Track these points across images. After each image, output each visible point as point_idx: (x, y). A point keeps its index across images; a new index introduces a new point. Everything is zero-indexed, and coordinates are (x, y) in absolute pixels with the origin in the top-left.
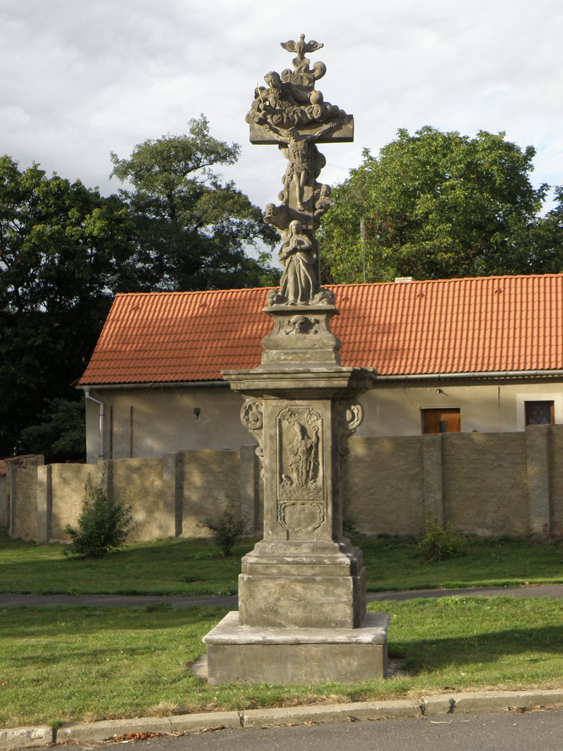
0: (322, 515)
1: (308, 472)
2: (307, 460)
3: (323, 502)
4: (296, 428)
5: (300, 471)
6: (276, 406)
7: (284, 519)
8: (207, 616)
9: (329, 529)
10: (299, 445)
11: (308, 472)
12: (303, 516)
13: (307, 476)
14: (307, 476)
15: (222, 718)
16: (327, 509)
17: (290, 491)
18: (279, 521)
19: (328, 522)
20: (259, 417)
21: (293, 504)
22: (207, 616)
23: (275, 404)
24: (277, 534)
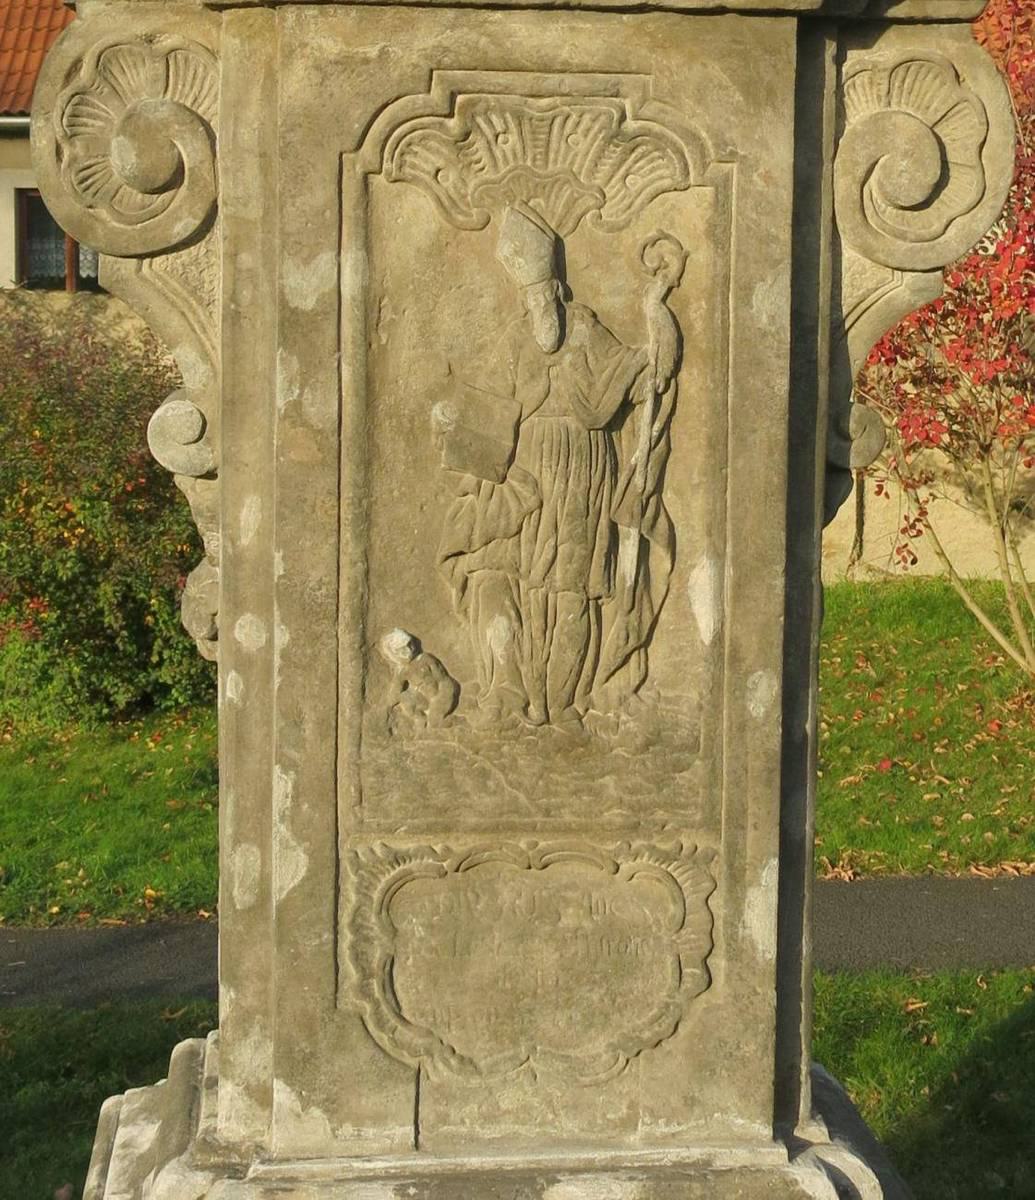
0: (692, 938)
1: (592, 608)
2: (587, 511)
3: (703, 841)
4: (504, 250)
5: (531, 601)
6: (344, 63)
7: (389, 984)
8: (674, 317)
9: (750, 1048)
10: (529, 394)
11: (592, 608)
12: (546, 958)
13: (588, 640)
14: (588, 640)
15: (816, 485)
16: (736, 904)
17: (442, 764)
18: (349, 1000)
19: (739, 1006)
20: (190, 150)
21: (465, 865)
22: (674, 317)
23: (332, 47)
24: (332, 1107)
